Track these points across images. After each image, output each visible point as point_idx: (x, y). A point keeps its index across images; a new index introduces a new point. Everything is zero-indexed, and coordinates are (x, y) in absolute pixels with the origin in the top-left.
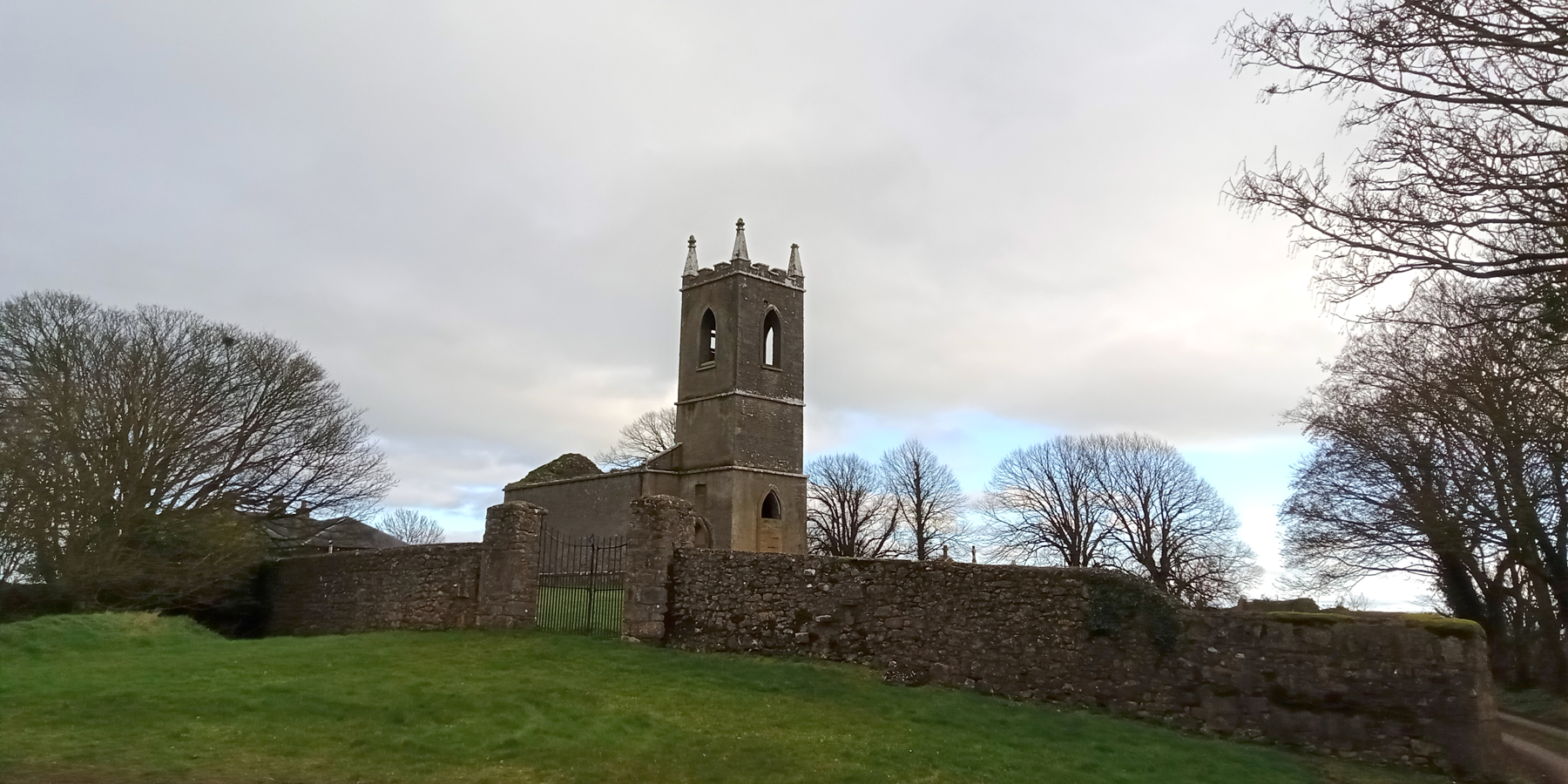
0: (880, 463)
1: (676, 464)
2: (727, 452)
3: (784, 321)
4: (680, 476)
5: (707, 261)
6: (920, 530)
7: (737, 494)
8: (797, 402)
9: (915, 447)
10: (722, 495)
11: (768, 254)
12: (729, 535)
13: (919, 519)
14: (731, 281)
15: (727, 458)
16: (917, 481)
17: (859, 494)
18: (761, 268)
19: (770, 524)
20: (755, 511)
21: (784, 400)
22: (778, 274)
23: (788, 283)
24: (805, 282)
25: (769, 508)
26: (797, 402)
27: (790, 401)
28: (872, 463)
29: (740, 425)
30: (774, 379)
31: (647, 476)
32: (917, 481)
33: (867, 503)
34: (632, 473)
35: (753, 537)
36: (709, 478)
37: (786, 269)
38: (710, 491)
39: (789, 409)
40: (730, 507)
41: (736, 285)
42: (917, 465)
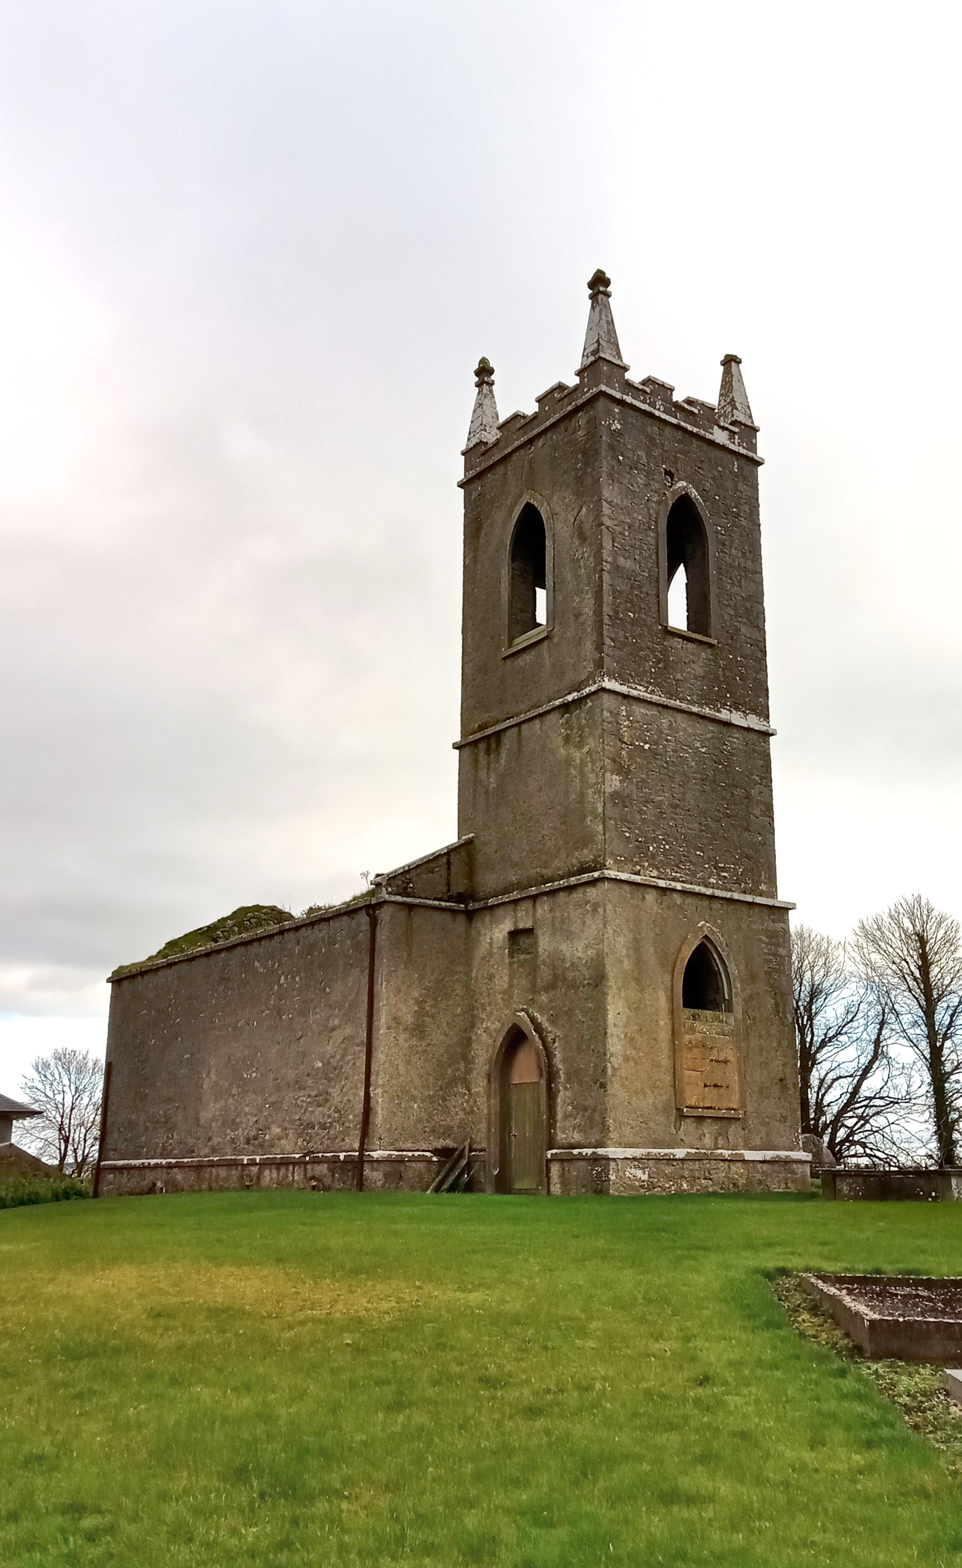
0: (852, 938)
1: (459, 886)
2: (586, 840)
3: (713, 527)
4: (470, 916)
5: (517, 397)
6: (935, 1062)
7: (618, 944)
8: (753, 721)
9: (918, 910)
10: (576, 950)
11: (670, 355)
12: (602, 1055)
13: (932, 1036)
14: (582, 419)
15: (587, 855)
16: (925, 968)
17: (815, 993)
18: (657, 389)
19: (706, 1026)
20: (663, 993)
21: (724, 715)
22: (692, 410)
23: (720, 437)
24: (761, 439)
25: (701, 984)
26: (753, 721)
27: (736, 718)
28: (836, 937)
29: (621, 770)
30: (696, 663)
31: (384, 915)
32: (925, 968)
33: (829, 1014)
34: (349, 911)
35: (664, 1060)
36: (543, 908)
37: (711, 397)
38: (545, 943)
39: (736, 739)
40: (598, 980)
41: (593, 424)
42: (922, 940)
